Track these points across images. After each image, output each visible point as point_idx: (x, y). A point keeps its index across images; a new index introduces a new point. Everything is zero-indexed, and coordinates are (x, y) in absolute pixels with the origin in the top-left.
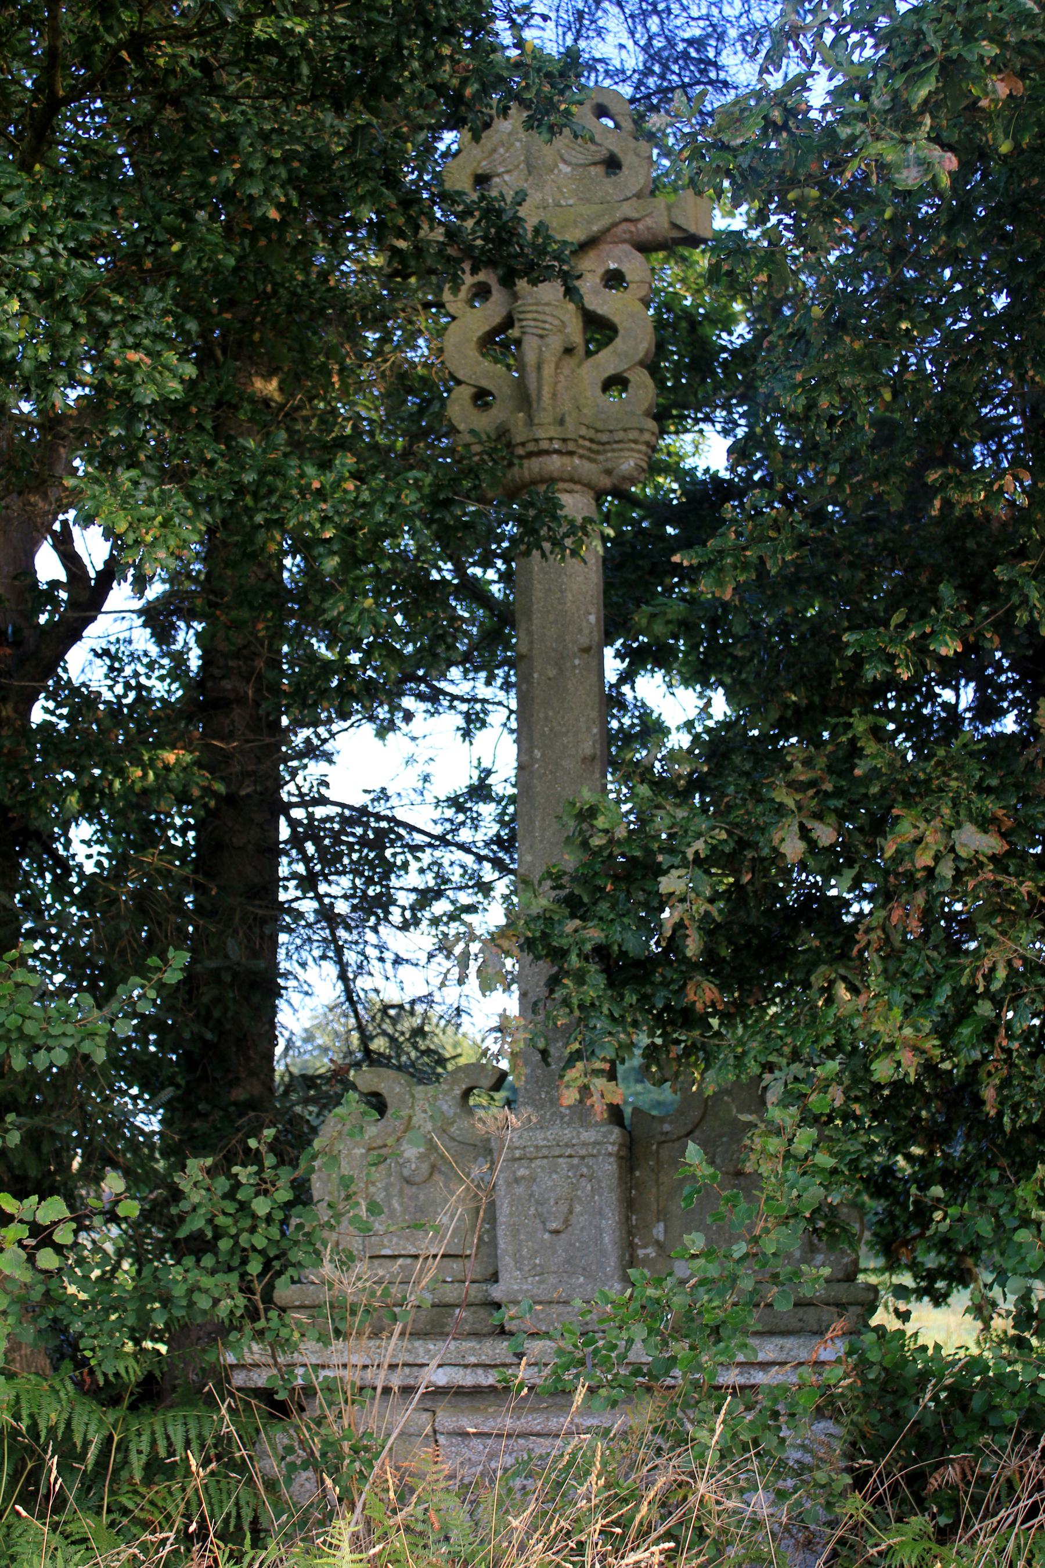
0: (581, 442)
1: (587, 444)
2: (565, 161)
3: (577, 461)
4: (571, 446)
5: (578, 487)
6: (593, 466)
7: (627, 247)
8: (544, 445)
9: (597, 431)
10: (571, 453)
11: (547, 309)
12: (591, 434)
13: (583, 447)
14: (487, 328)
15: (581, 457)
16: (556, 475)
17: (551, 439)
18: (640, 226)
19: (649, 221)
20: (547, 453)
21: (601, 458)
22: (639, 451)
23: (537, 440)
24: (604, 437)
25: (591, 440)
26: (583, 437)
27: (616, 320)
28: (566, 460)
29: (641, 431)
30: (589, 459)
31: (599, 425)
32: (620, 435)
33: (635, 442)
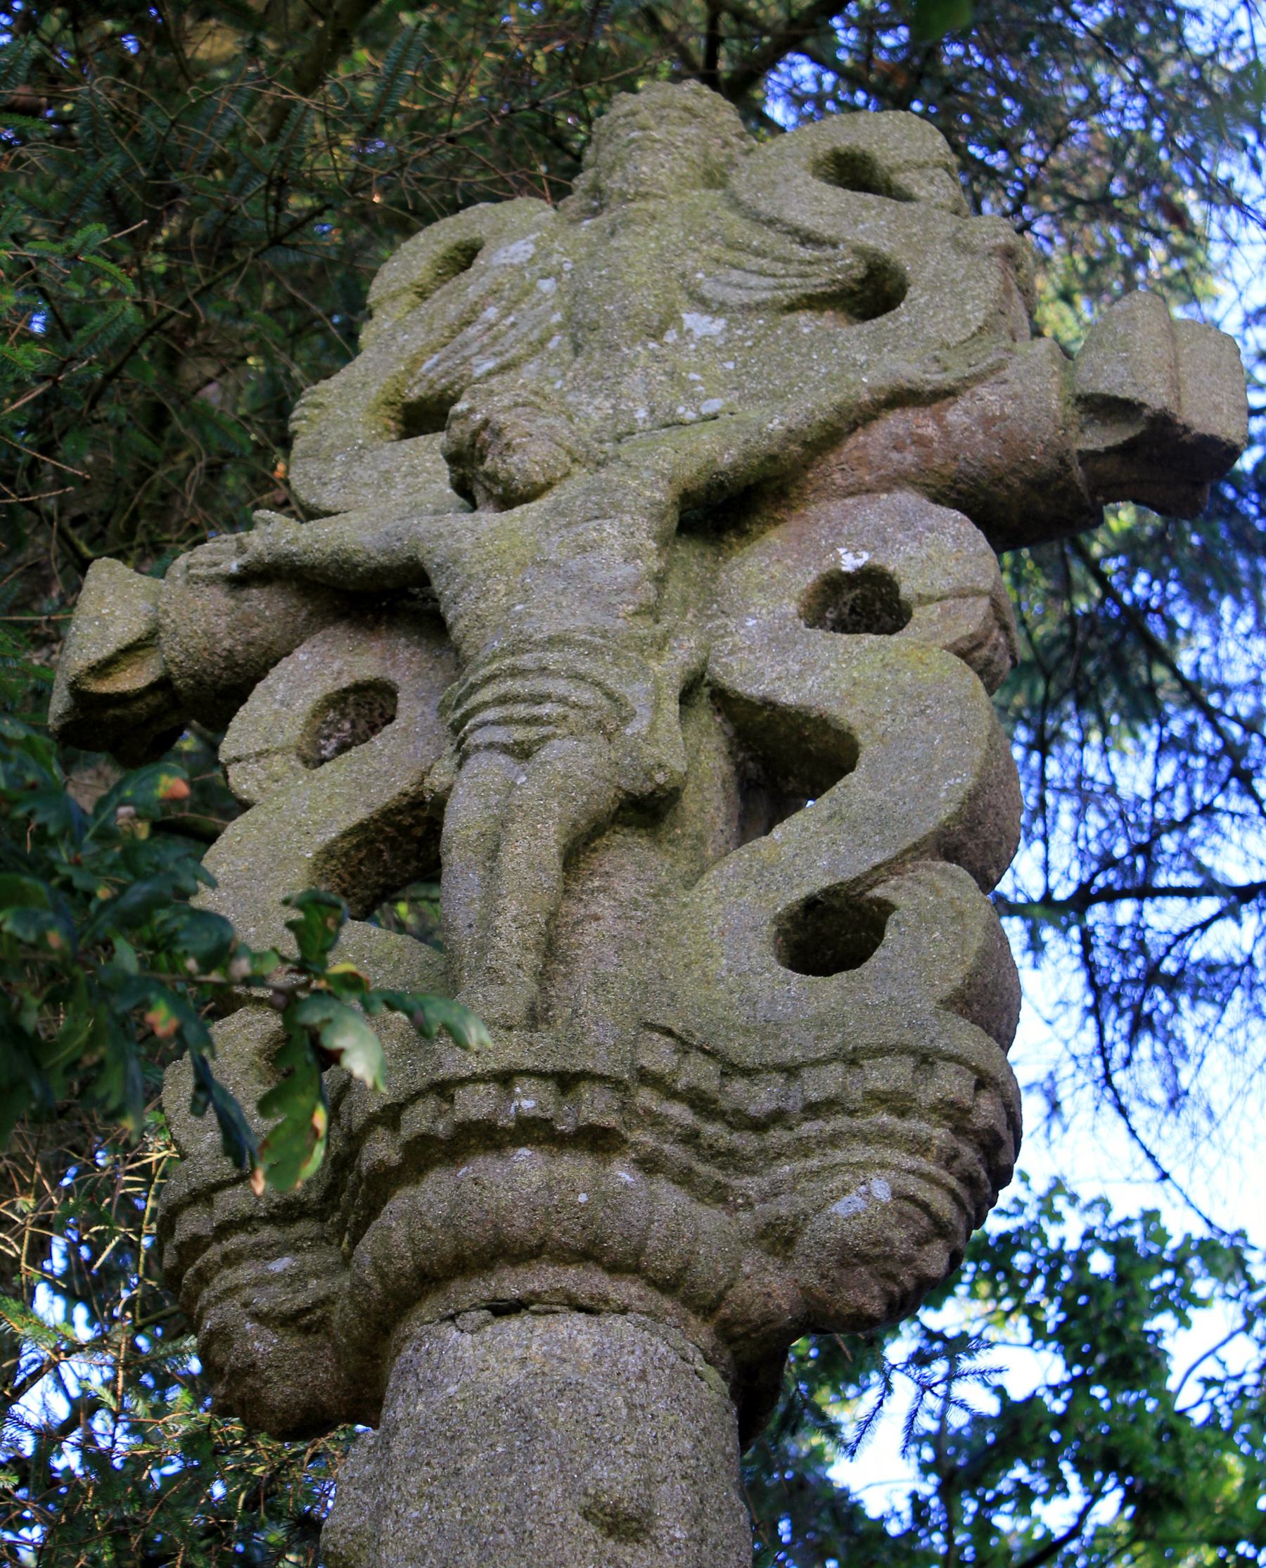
0: (646, 1098)
1: (679, 1112)
2: (703, 304)
3: (623, 1173)
4: (595, 1107)
5: (627, 1290)
6: (710, 1217)
7: (908, 499)
8: (476, 1103)
9: (731, 1070)
10: (598, 1141)
11: (552, 658)
12: (698, 1073)
13: (656, 1121)
14: (361, 814)
15: (649, 1165)
16: (519, 1225)
17: (505, 1079)
18: (955, 415)
19: (989, 397)
20: (485, 1137)
21: (750, 1184)
22: (919, 1146)
23: (443, 1089)
24: (761, 1097)
25: (700, 1102)
26: (645, 1077)
27: (849, 716)
28: (575, 1167)
29: (925, 1059)
30: (685, 1178)
31: (745, 1050)
32: (827, 1081)
33: (899, 1104)
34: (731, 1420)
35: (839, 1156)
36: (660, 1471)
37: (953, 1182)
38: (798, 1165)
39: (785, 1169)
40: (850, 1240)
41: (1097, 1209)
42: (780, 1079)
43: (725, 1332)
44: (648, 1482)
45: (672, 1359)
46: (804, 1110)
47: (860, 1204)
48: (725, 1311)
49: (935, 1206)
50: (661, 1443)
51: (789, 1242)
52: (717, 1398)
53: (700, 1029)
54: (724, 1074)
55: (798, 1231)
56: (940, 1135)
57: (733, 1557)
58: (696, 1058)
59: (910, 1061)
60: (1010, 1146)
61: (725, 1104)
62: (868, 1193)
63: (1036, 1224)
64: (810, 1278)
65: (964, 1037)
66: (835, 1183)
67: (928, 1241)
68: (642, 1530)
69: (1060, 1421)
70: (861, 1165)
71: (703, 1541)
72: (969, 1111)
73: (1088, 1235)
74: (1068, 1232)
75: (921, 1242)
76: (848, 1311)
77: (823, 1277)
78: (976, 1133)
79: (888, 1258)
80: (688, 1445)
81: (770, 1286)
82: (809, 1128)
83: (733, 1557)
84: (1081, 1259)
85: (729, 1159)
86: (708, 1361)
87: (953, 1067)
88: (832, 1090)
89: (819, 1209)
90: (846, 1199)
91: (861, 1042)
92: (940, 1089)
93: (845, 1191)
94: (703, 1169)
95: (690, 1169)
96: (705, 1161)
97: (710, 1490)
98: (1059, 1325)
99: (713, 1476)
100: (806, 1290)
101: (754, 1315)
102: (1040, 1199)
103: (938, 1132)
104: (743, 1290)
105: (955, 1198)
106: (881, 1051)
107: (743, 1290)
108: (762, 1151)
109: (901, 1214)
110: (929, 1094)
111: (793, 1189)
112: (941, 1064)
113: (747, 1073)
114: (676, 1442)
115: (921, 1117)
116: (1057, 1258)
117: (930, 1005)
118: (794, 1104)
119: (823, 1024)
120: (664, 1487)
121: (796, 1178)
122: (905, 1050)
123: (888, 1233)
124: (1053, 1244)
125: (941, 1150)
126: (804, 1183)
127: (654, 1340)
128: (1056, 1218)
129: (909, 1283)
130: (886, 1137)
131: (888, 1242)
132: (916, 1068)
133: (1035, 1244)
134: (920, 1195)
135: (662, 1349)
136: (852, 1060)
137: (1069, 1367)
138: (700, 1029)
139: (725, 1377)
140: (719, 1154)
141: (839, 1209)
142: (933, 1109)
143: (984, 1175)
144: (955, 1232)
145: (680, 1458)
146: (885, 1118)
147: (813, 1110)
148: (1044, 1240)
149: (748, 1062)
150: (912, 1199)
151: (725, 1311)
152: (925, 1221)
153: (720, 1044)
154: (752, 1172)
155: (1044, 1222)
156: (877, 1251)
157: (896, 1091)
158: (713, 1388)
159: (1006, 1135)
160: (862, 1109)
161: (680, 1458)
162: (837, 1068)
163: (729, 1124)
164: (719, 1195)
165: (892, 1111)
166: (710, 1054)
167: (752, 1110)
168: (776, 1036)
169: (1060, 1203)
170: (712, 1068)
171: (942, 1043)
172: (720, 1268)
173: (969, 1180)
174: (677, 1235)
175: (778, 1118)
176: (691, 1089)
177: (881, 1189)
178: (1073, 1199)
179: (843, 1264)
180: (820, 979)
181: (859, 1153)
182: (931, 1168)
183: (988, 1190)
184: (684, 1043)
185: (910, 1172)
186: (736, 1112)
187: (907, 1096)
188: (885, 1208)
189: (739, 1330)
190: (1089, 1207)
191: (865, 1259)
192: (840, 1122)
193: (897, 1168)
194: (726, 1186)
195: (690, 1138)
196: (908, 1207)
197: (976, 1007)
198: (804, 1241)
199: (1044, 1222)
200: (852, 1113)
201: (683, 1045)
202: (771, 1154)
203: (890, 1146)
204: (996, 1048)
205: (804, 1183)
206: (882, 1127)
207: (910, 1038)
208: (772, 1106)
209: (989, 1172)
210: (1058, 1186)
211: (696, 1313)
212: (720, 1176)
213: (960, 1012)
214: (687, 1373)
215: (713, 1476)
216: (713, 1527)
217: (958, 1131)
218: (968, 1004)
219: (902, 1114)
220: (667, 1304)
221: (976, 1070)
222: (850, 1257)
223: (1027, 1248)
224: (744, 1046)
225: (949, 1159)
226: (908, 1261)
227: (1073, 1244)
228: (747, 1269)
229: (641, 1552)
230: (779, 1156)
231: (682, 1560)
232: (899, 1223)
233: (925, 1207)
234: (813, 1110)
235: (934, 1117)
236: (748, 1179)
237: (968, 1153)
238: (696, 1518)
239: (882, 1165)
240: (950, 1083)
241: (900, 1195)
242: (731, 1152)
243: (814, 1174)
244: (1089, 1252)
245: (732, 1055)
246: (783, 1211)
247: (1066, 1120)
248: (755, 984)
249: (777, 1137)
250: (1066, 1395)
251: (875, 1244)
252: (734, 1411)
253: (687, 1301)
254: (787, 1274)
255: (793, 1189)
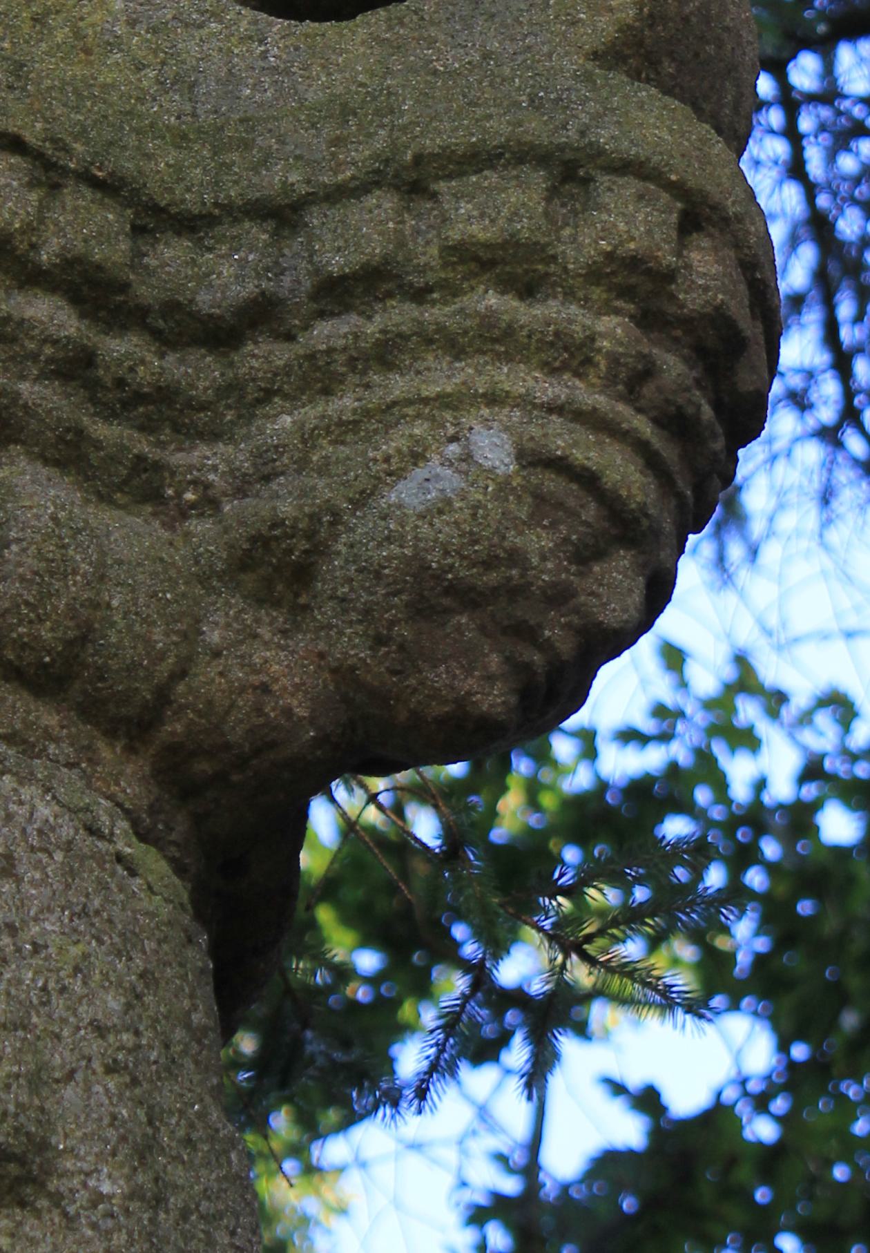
1: (46, 311)
6: (129, 533)
9: (155, 219)
12: (82, 227)
21: (211, 460)
22: (570, 355)
24: (224, 275)
25: (91, 289)
29: (572, 173)
30: (69, 454)
31: (185, 177)
32: (364, 231)
33: (518, 267)
34: (198, 958)
35: (399, 385)
36: (58, 1059)
37: (643, 426)
38: (311, 413)
39: (283, 423)
40: (434, 560)
41: (824, 720)
42: (260, 234)
43: (178, 776)
44: (37, 1080)
45: (66, 832)
46: (315, 296)
47: (450, 481)
48: (174, 728)
49: (611, 478)
50: (59, 1003)
51: (302, 575)
52: (166, 911)
53: (82, 134)
54: (138, 230)
55: (319, 550)
56: (612, 329)
57: (223, 1238)
58: (77, 198)
59: (539, 179)
60: (759, 354)
61: (145, 293)
62: (467, 457)
63: (705, 758)
64: (351, 645)
65: (651, 123)
66: (396, 442)
67: (599, 555)
68: (30, 1179)
69: (770, 1160)
70: (446, 401)
71: (158, 1202)
72: (669, 276)
73: (812, 771)
74: (770, 768)
75: (586, 555)
76: (438, 709)
77: (380, 641)
78: (687, 323)
79: (515, 592)
80: (114, 1002)
81: (265, 667)
82: (328, 333)
83: (223, 1238)
84: (800, 818)
85: (161, 408)
86: (143, 837)
87: (630, 186)
88: (376, 248)
89: (361, 501)
90: (420, 473)
91: (431, 144)
92: (607, 232)
93: (417, 457)
94: (103, 430)
95: (80, 432)
96: (110, 414)
97: (167, 1096)
98: (760, 960)
99: (171, 1068)
100: (344, 673)
101: (235, 731)
102: (708, 705)
103: (607, 323)
104: (209, 679)
105: (651, 461)
106: (477, 159)
107: (209, 679)
108: (231, 389)
109: (540, 498)
110: (582, 244)
111: (302, 464)
112: (604, 180)
113: (191, 225)
114: (90, 997)
115: (570, 295)
116: (756, 817)
117: (573, 63)
118: (295, 283)
119: (346, 112)
120: (70, 1092)
121: (308, 439)
122: (522, 155)
123: (514, 539)
124: (740, 791)
125: (614, 359)
126: (326, 448)
127: (26, 792)
128: (747, 740)
129: (566, 646)
130: (497, 340)
131: (515, 557)
132: (552, 193)
133: (702, 795)
134: (578, 456)
135: (45, 811)
136: (414, 181)
137: (783, 1046)
138: (82, 134)
139: (179, 869)
140: (140, 398)
141: (408, 493)
142: (594, 275)
143: (707, 412)
144: (656, 533)
145: (100, 1030)
146: (492, 300)
147: (336, 293)
148: (720, 784)
149: (191, 202)
150: (560, 465)
151: (174, 728)
152: (591, 512)
153: (129, 166)
154: (214, 435)
155: (719, 749)
156: (493, 578)
157: (511, 244)
158: (155, 891)
159: (751, 329)
160: (443, 285)
161: (100, 1030)
162: (383, 203)
163: (156, 334)
164: (144, 486)
165: (507, 285)
166: (109, 187)
167: (205, 301)
168: (246, 145)
169: (748, 711)
170: (111, 217)
171: (603, 136)
172: (157, 634)
173: (677, 423)
174: (61, 569)
175: (261, 315)
176: (71, 262)
177: (493, 448)
178: (776, 700)
179: (422, 610)
180: (329, 28)
181: (441, 376)
182: (600, 401)
183: (719, 445)
184: (49, 165)
185: (554, 408)
186: (172, 308)
187: (539, 251)
188: (504, 487)
189: (203, 767)
190: (806, 719)
191: (468, 597)
192: (397, 315)
193: (525, 402)
194: (158, 467)
195: (75, 367)
196: (552, 483)
197: (669, 68)
198: (336, 569)
199: (719, 749)
200: (420, 295)
201: (48, 170)
202: (252, 393)
203: (508, 358)
204: (719, 147)
205: (326, 448)
206: (488, 319)
207: (536, 129)
208: (247, 290)
209: (717, 406)
210: (744, 679)
211: (111, 734)
212: (143, 446)
213: (635, 75)
214: (100, 859)
215: (171, 1068)
216: (178, 1174)
217: (649, 320)
218: (652, 61)
219: (528, 290)
220: (50, 719)
221: (679, 190)
222: (436, 593)
223: (685, 807)
224: (178, 168)
225: (634, 380)
226: (559, 596)
227: (782, 789)
228: (215, 637)
229: (31, 1227)
230: (268, 395)
231: (119, 1239)
232: (534, 520)
233: (588, 480)
234: (336, 293)
235: (597, 293)
236: (203, 449)
237: (673, 367)
238: (144, 1152)
239: (493, 399)
240: (627, 220)
241: (533, 458)
242: (165, 395)
243: (345, 428)
244: (815, 807)
245: (153, 187)
246: (286, 509)
247: (757, 527)
248: (190, 47)
249: (261, 356)
250: (780, 1105)
251: (489, 563)
252: (203, 939)
253: (90, 710)
254: (301, 642)
255: (302, 464)
